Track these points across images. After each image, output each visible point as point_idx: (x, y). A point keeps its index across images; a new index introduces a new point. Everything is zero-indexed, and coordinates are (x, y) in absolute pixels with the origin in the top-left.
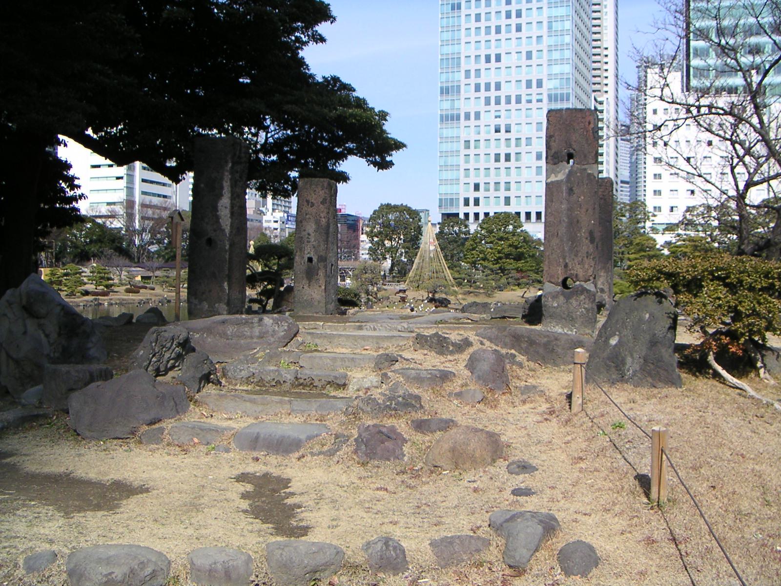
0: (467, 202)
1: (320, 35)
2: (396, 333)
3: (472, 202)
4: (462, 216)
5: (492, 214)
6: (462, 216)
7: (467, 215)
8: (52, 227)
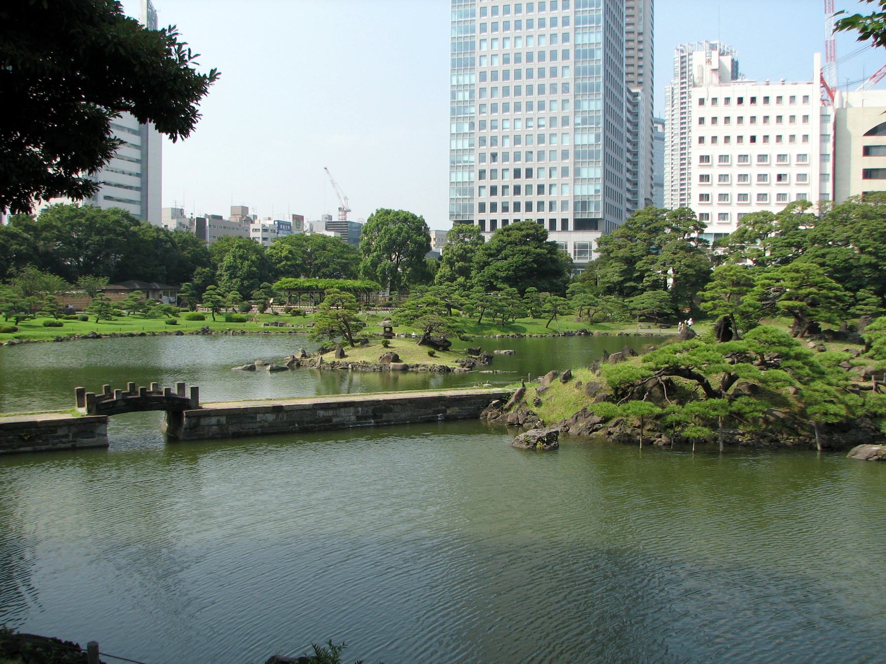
0: (482, 207)
1: (119, 139)
2: (412, 593)
3: (488, 208)
4: (476, 223)
5: (511, 222)
6: (476, 223)
7: (482, 223)
8: (13, 266)
